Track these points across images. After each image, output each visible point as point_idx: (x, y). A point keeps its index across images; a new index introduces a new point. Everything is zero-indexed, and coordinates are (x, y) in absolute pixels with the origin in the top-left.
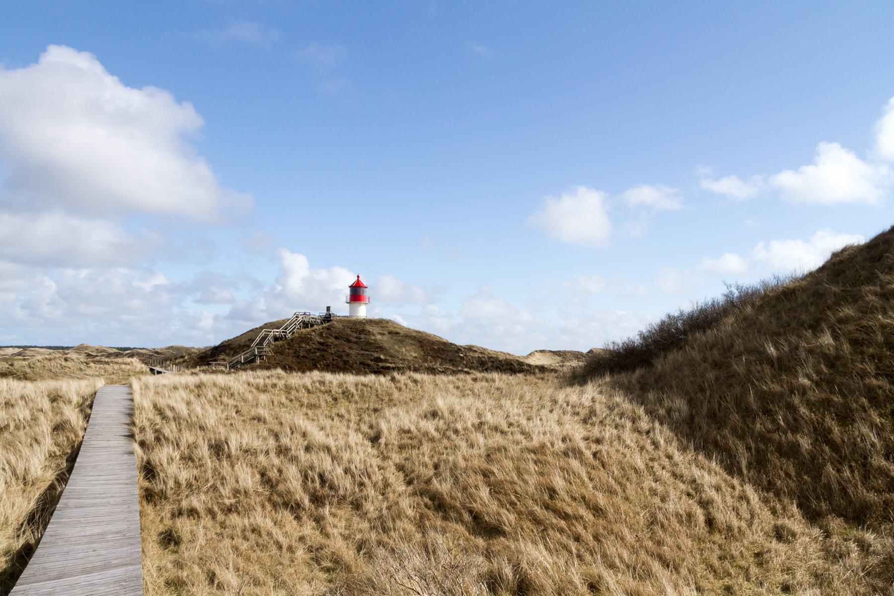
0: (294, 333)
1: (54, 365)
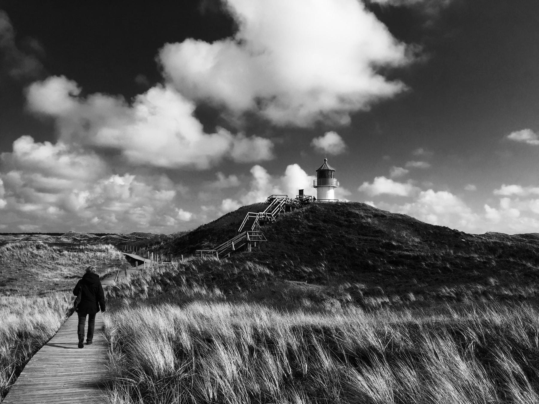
0: (278, 216)
1: (25, 254)
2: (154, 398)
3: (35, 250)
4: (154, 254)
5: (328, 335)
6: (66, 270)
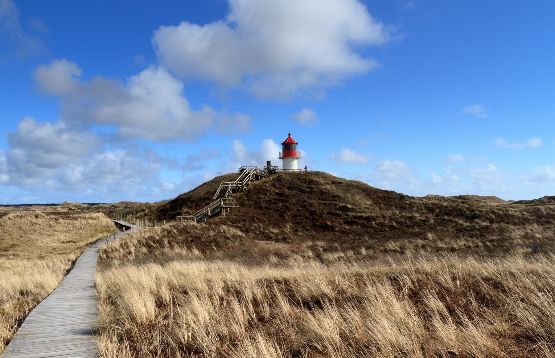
0: (248, 185)
1: (24, 222)
2: (137, 341)
3: (34, 219)
4: (139, 220)
5: (288, 285)
6: (62, 236)
